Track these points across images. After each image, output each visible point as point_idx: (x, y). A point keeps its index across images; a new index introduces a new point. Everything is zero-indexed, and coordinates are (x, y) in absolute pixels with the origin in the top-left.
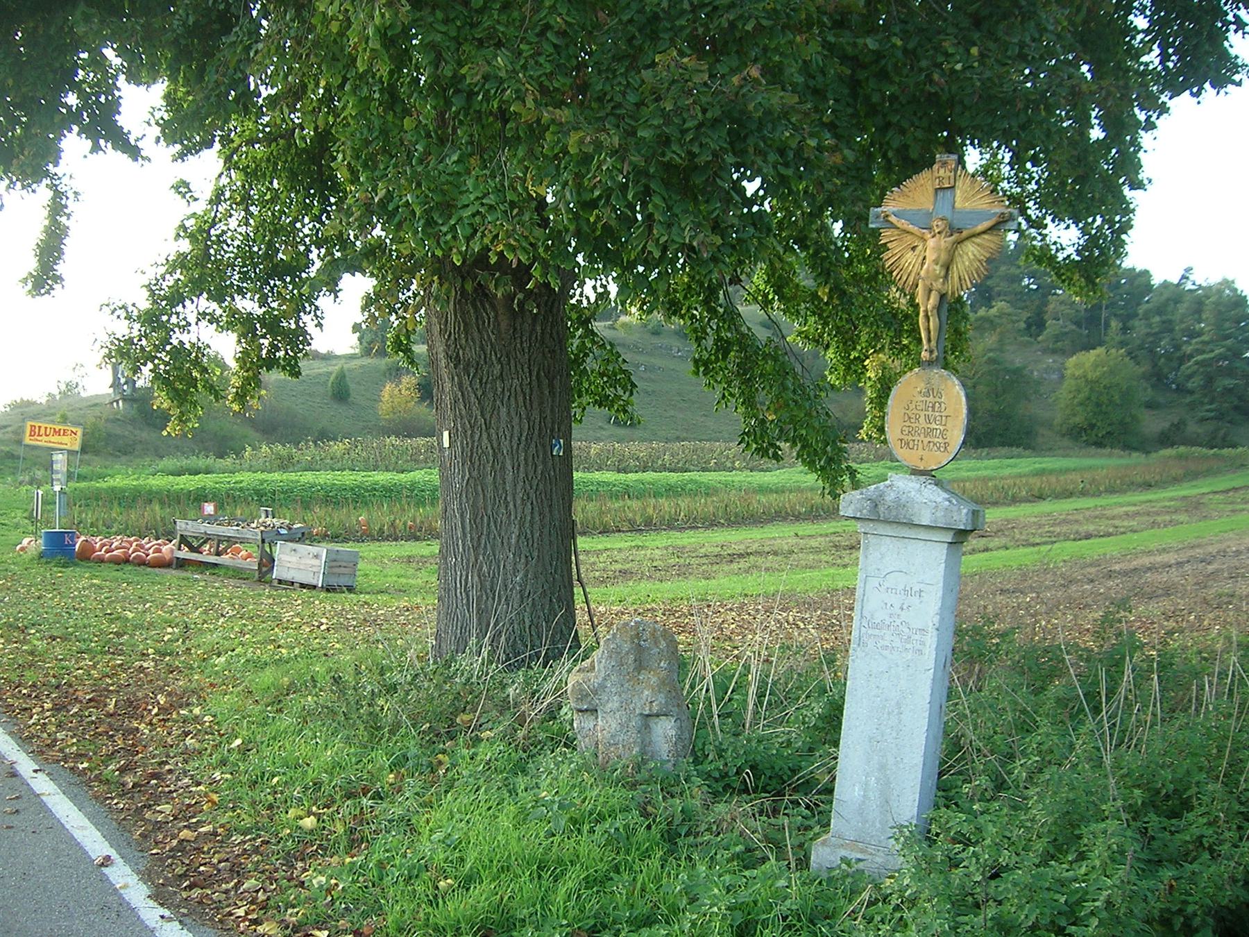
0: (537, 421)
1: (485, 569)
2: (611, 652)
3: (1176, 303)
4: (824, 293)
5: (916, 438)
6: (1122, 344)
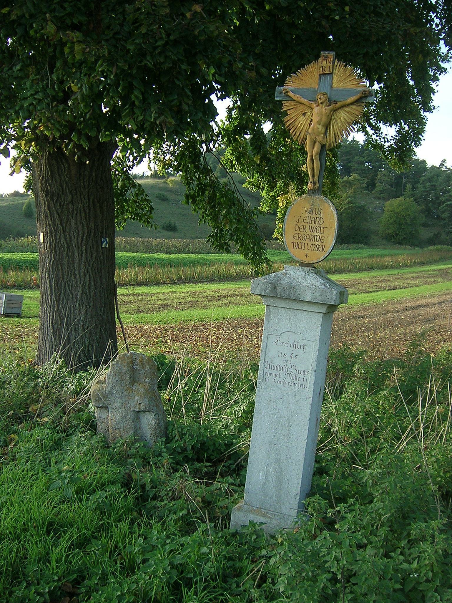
0: (93, 228)
1: (63, 312)
2: (115, 372)
3: (438, 177)
4: (257, 159)
5: (304, 241)
6: (412, 195)
